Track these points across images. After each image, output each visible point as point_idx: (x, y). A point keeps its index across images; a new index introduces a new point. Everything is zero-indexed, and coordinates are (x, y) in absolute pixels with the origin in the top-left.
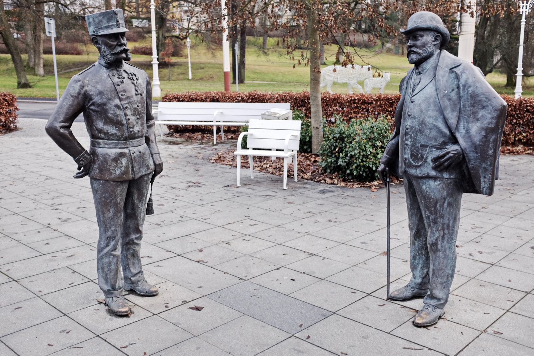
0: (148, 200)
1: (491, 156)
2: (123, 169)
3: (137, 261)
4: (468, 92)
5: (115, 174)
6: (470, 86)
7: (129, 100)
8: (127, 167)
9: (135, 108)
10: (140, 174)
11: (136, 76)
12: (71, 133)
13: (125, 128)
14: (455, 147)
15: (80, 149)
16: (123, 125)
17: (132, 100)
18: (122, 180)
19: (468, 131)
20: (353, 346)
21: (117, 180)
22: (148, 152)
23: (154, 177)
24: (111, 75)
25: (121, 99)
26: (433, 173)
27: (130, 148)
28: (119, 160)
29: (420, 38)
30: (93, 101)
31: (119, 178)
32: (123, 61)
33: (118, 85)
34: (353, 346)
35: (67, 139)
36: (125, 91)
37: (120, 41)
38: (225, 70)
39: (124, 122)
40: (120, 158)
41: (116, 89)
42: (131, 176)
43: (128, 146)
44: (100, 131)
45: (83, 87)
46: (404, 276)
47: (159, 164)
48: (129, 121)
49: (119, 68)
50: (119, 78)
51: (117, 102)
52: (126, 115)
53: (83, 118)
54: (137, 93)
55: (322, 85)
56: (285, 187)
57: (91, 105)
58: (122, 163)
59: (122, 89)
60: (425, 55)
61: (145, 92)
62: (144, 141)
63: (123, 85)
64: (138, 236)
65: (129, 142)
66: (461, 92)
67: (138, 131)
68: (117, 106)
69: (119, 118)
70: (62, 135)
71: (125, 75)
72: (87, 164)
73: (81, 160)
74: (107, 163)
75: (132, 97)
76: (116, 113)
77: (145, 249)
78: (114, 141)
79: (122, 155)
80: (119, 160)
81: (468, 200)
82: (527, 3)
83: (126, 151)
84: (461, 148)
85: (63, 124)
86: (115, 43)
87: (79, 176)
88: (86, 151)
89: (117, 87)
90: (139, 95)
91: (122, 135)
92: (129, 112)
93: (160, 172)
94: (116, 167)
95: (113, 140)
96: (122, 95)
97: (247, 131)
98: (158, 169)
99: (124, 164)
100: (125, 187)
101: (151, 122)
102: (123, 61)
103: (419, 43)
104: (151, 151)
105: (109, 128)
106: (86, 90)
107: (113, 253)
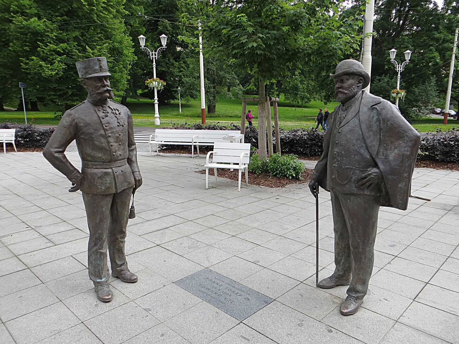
0: (130, 207)
1: (406, 178)
4: (387, 125)
5: (101, 189)
6: (388, 121)
9: (118, 137)
10: (122, 189)
11: (118, 111)
12: (65, 157)
14: (375, 170)
18: (107, 194)
19: (386, 157)
20: (290, 335)
21: (103, 194)
22: (129, 170)
23: (134, 189)
24: (97, 110)
26: (355, 190)
27: (113, 168)
29: (347, 81)
30: (83, 131)
31: (104, 192)
32: (108, 100)
33: (103, 118)
34: (290, 335)
35: (63, 162)
36: (108, 123)
37: (104, 83)
38: (202, 108)
41: (101, 122)
42: (113, 191)
44: (89, 155)
45: (74, 120)
46: (329, 268)
47: (139, 180)
49: (104, 104)
50: (103, 113)
51: (102, 132)
53: (75, 144)
54: (119, 124)
55: (279, 125)
56: (239, 190)
57: (81, 135)
59: (106, 122)
60: (351, 94)
61: (127, 124)
62: (127, 162)
63: (107, 118)
67: (120, 155)
70: (57, 158)
71: (109, 110)
72: (80, 181)
73: (73, 179)
74: (94, 180)
75: (115, 128)
77: (131, 243)
81: (385, 214)
82: (401, 65)
83: (110, 170)
84: (380, 170)
85: (57, 149)
86: (100, 85)
87: (73, 190)
88: (78, 170)
89: (102, 120)
90: (122, 126)
92: (111, 140)
93: (139, 186)
95: (99, 162)
96: (106, 126)
97: (213, 151)
98: (138, 183)
100: (109, 200)
101: (133, 147)
102: (108, 100)
103: (345, 85)
104: (132, 170)
105: (95, 153)
106: (77, 123)
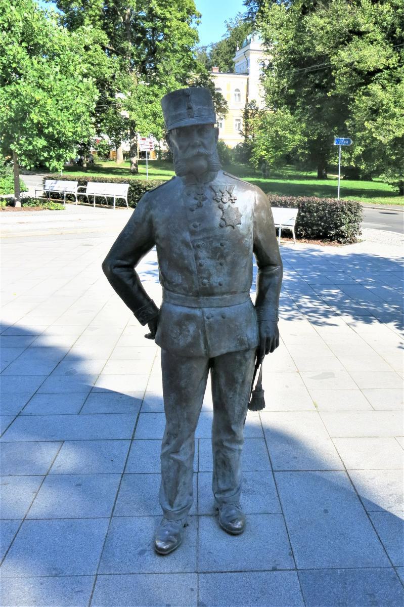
2: (189, 339)
3: (228, 473)
7: (205, 235)
8: (196, 338)
13: (194, 277)
15: (141, 297)
16: (191, 272)
17: (211, 235)
25: (193, 233)
27: (205, 310)
28: (186, 326)
39: (194, 268)
40: (187, 323)
43: (202, 305)
48: (202, 268)
52: (197, 258)
58: (188, 331)
64: (229, 438)
65: (203, 299)
68: (186, 244)
69: (186, 262)
76: (182, 253)
78: (180, 295)
79: (189, 318)
80: (186, 326)
83: (198, 312)
91: (191, 288)
92: (203, 254)
94: (180, 334)
95: (179, 293)
99: (191, 332)
107: (172, 455)
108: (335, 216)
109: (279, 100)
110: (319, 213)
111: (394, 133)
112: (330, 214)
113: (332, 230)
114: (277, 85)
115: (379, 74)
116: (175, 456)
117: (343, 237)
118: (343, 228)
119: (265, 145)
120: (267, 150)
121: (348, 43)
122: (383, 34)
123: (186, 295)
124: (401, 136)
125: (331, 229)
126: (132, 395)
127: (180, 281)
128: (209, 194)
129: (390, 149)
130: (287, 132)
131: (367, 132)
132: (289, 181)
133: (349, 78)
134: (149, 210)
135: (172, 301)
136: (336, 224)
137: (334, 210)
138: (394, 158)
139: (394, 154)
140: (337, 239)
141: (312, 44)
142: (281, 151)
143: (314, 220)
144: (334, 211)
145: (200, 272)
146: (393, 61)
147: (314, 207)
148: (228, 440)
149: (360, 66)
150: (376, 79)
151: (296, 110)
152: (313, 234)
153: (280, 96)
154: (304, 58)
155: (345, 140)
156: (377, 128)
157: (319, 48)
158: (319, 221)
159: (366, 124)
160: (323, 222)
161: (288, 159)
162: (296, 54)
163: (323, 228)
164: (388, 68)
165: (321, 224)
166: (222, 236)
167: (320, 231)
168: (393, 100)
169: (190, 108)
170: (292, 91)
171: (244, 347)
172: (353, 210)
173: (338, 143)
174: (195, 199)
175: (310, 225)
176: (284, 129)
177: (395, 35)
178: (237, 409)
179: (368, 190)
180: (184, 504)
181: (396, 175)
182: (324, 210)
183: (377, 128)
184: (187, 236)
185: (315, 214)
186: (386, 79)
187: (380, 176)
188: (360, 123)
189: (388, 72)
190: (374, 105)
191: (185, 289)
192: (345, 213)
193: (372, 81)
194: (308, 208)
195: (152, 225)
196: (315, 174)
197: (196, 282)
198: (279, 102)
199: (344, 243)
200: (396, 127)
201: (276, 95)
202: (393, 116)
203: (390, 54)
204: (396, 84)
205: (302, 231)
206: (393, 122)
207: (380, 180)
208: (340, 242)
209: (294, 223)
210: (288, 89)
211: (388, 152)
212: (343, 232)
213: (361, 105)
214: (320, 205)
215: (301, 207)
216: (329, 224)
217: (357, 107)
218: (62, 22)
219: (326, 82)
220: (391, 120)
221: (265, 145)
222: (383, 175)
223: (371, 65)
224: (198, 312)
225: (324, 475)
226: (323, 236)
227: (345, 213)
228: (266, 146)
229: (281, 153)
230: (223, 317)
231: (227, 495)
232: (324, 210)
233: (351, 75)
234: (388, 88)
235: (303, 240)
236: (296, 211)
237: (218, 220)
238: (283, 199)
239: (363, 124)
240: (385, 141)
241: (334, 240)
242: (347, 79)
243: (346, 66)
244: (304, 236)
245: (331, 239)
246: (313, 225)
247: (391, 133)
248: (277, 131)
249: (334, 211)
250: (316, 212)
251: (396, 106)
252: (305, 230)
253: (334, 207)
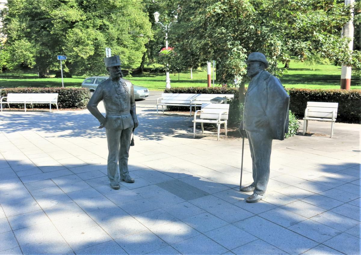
2: (119, 125)
8: (120, 124)
16: (119, 105)
26: (255, 129)
52: (120, 101)
58: (118, 122)
65: (122, 113)
66: (268, 90)
68: (116, 97)
79: (118, 118)
83: (120, 117)
92: (121, 100)
108: (77, 96)
109: (21, 34)
110: (69, 95)
111: (89, 53)
112: (74, 95)
113: (77, 103)
114: (19, 26)
115: (77, 23)
116: (114, 161)
117: (82, 105)
118: (82, 101)
119: (5, 59)
120: (7, 62)
121: (59, 6)
122: (77, 3)
123: (117, 112)
124: (92, 55)
125: (76, 102)
126: (58, 166)
127: (115, 108)
128: (120, 84)
129: (87, 61)
130: (29, 52)
131: (75, 52)
132: (23, 80)
133: (62, 24)
134: (102, 89)
135: (112, 115)
136: (78, 100)
137: (76, 93)
138: (89, 66)
139: (89, 64)
140: (80, 107)
141: (38, 5)
142: (16, 62)
143: (66, 99)
144: (77, 93)
145: (121, 105)
146: (84, 18)
147: (65, 92)
148: (126, 156)
149: (67, 19)
150: (76, 26)
151: (31, 41)
152: (66, 105)
153: (22, 32)
154: (33, 12)
155: (63, 57)
156: (80, 51)
157: (43, 8)
158: (69, 99)
159: (74, 48)
160: (71, 99)
161: (24, 67)
162: (27, 9)
163: (72, 102)
164: (81, 20)
165: (70, 100)
166: (126, 95)
167: (70, 104)
168: (87, 37)
169: (117, 61)
170: (29, 30)
171: (131, 126)
172: (86, 92)
173: (59, 58)
174: (117, 85)
175: (64, 101)
176: (26, 50)
177: (83, 4)
178: (128, 146)
179: (68, 83)
180: (117, 176)
181: (92, 75)
182: (71, 93)
183: (80, 51)
184: (117, 95)
185: (67, 96)
186: (81, 26)
187: (83, 75)
188: (71, 48)
189: (82, 22)
190: (77, 39)
191: (117, 110)
192: (83, 94)
193: (74, 27)
194: (62, 93)
195: (254, 76)
196: (38, 75)
197: (120, 108)
198: (21, 36)
199: (83, 109)
200: (89, 50)
201: (19, 32)
202: (87, 45)
203: (82, 13)
204: (87, 29)
205: (60, 104)
206: (88, 47)
207: (84, 77)
208: (81, 108)
209: (56, 101)
210: (26, 29)
211: (86, 63)
212: (82, 103)
213: (70, 39)
214: (69, 91)
215: (61, 93)
216: (75, 100)
217: (68, 40)
218: (136, 51)
219: (47, 26)
220: (87, 47)
221: (5, 59)
222: (85, 75)
223: (74, 19)
224: (120, 117)
225: (145, 170)
226: (72, 106)
227: (83, 94)
228: (7, 60)
229: (17, 63)
230: (127, 117)
231: (126, 173)
232: (71, 93)
233: (62, 23)
234: (83, 31)
235: (61, 109)
236: (57, 94)
237: (124, 91)
238: (26, 88)
239: (72, 49)
240: (85, 57)
241: (78, 107)
242: (60, 25)
243: (60, 18)
244: (62, 107)
245: (77, 107)
246: (66, 101)
247: (87, 53)
248: (22, 52)
249: (77, 93)
250: (67, 94)
251: (88, 40)
252: (62, 104)
253: (77, 91)
